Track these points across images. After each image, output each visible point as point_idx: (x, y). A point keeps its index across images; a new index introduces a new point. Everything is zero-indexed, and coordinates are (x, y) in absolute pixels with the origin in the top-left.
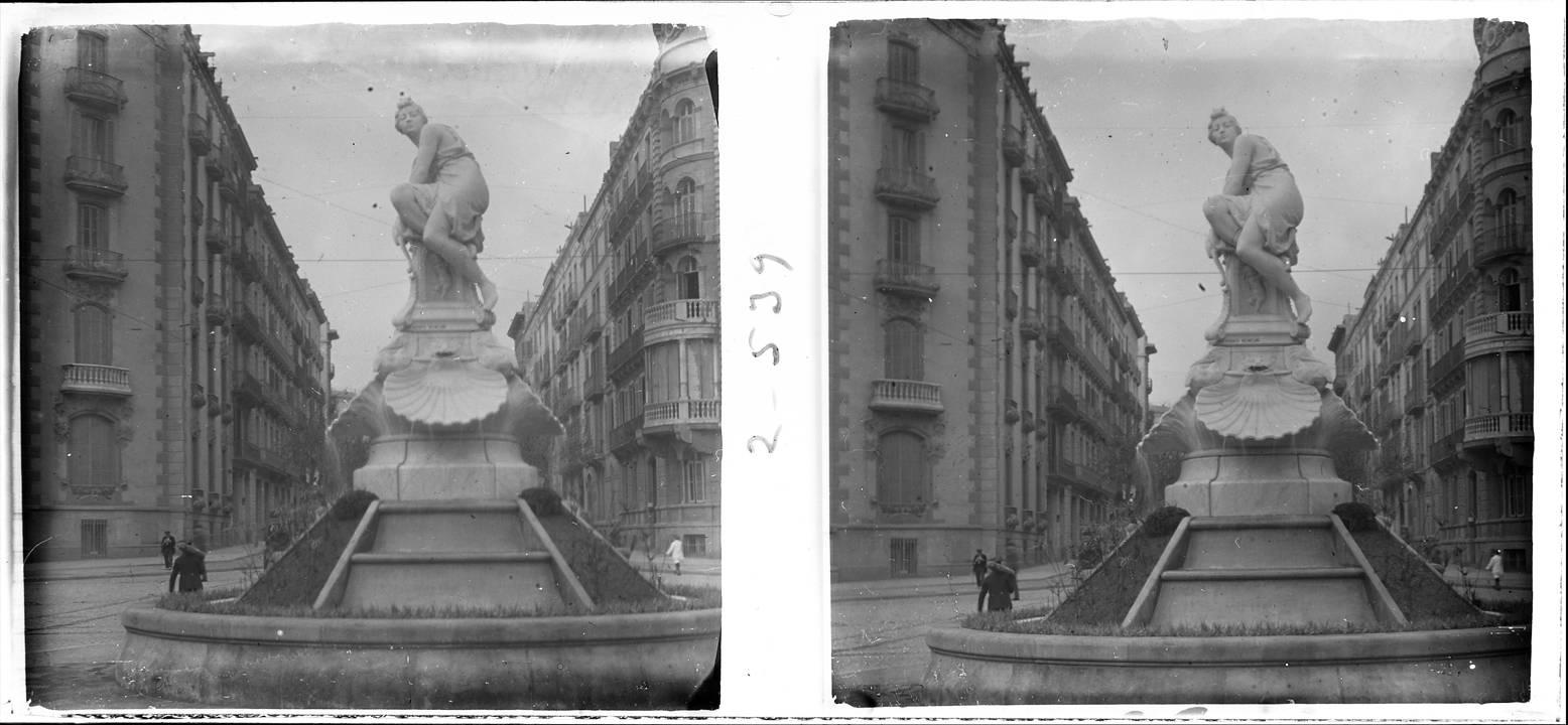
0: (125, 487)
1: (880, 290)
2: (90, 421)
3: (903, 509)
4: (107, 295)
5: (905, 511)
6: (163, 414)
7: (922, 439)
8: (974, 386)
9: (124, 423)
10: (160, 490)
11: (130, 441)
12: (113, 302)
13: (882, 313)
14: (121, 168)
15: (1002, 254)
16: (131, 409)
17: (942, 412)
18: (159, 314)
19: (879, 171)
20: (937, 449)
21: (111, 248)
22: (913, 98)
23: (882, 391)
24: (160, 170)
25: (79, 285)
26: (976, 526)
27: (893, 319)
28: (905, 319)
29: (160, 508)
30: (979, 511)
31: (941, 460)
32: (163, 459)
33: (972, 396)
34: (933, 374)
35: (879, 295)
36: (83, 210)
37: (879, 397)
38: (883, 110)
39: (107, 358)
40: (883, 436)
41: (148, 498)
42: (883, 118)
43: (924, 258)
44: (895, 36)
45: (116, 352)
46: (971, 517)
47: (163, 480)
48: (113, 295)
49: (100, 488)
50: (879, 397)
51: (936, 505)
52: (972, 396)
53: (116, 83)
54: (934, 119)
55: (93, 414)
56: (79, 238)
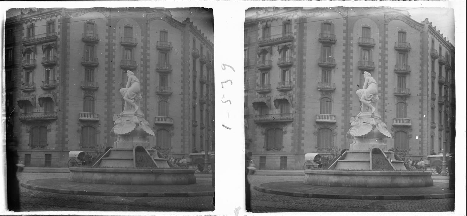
0: (410, 150)
1: (395, 96)
2: (401, 132)
3: (401, 151)
4: (405, 100)
5: (326, 150)
6: (183, 129)
7: (406, 133)
8: (183, 117)
9: (410, 133)
10: (420, 151)
11: (412, 138)
12: (169, 100)
13: (396, 101)
14: (410, 66)
15: (191, 83)
16: (412, 129)
17: (411, 126)
18: (420, 104)
19: (395, 65)
20: (410, 136)
21: (407, 88)
22: (166, 45)
23: (157, 119)
24: (422, 65)
25: (398, 98)
26: (421, 156)
27: (160, 101)
28: (164, 101)
29: (420, 156)
30: (422, 152)
31: (411, 138)
32: (183, 141)
33: (182, 120)
34: (409, 115)
35: (395, 97)
36: (399, 78)
37: (394, 123)
38: (396, 50)
39: (406, 116)
40: (396, 132)
41: (178, 151)
42: (397, 52)
43: (169, 85)
44: (161, 30)
45: (408, 115)
46: (420, 153)
47: (183, 147)
48: (407, 100)
49: (403, 150)
50: (394, 123)
51: (410, 150)
52: (182, 120)
53: (408, 44)
54: (171, 50)
55: (402, 131)
56: (398, 85)
